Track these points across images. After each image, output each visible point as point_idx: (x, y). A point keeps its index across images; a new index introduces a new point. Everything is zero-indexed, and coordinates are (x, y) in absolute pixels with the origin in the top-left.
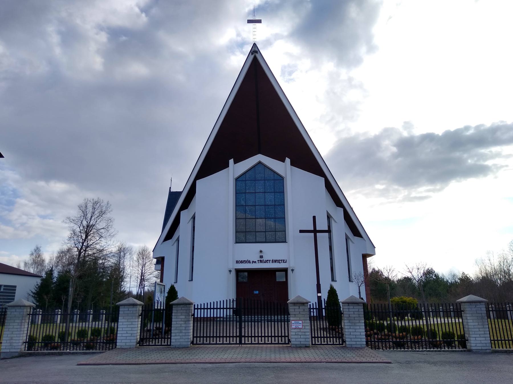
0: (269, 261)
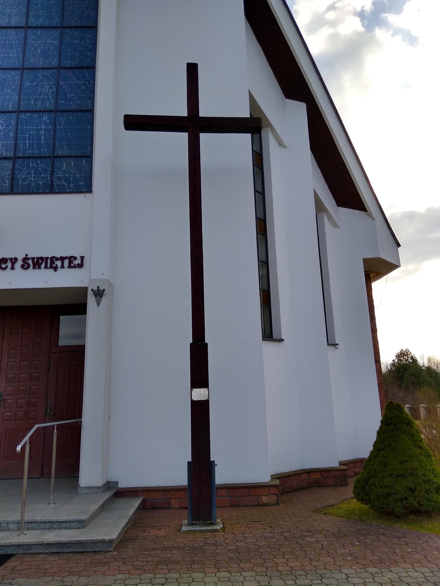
0: (9, 264)
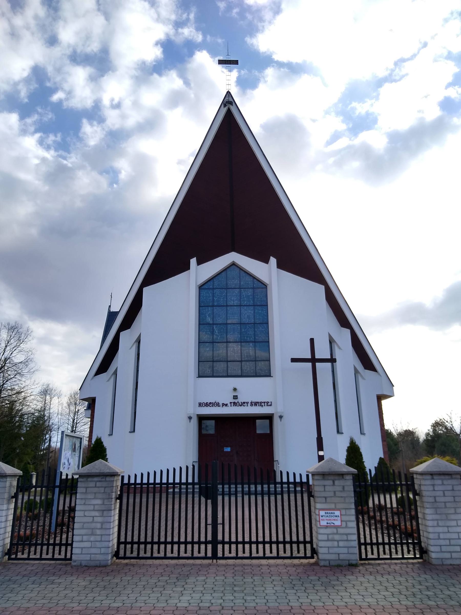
0: (246, 404)
